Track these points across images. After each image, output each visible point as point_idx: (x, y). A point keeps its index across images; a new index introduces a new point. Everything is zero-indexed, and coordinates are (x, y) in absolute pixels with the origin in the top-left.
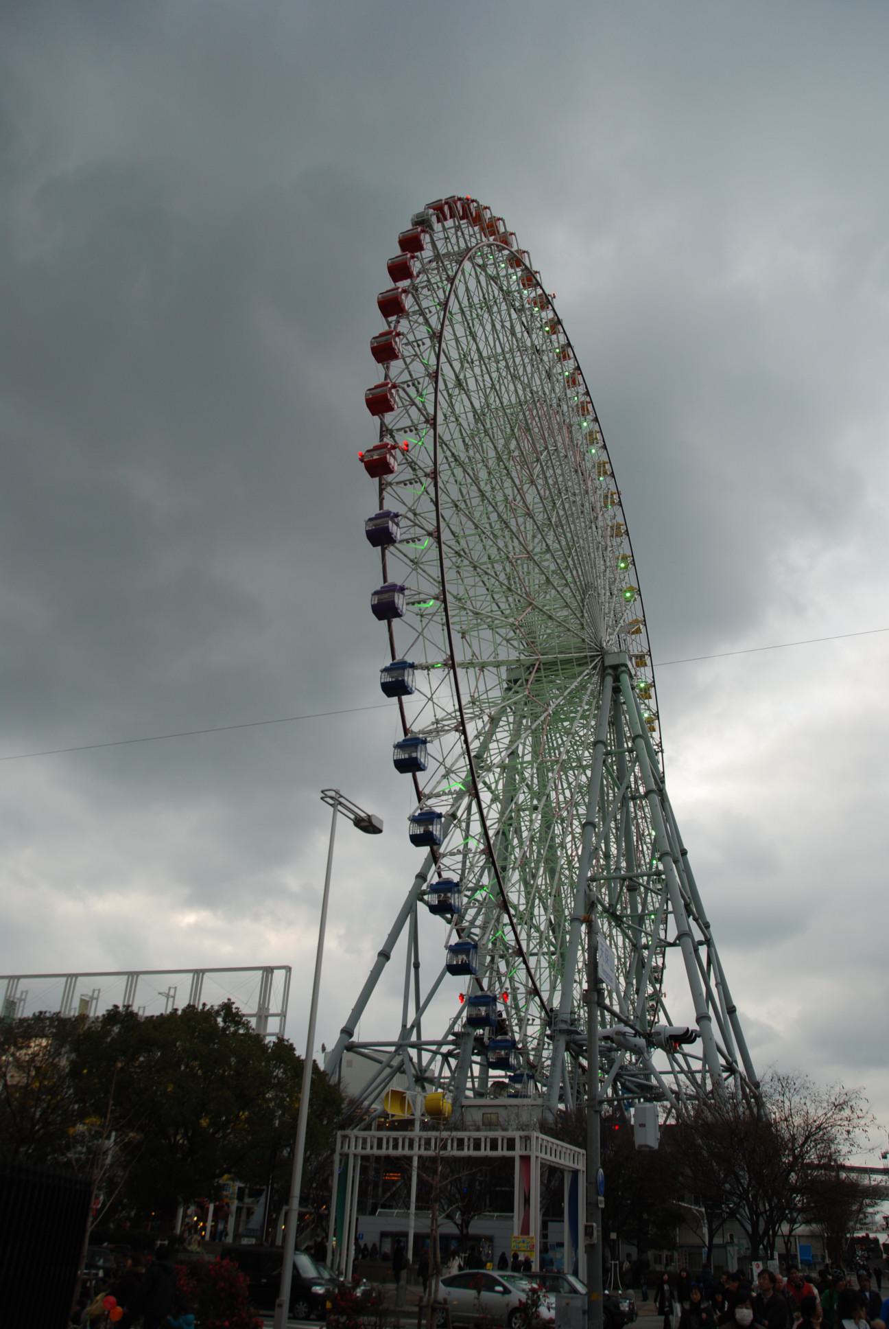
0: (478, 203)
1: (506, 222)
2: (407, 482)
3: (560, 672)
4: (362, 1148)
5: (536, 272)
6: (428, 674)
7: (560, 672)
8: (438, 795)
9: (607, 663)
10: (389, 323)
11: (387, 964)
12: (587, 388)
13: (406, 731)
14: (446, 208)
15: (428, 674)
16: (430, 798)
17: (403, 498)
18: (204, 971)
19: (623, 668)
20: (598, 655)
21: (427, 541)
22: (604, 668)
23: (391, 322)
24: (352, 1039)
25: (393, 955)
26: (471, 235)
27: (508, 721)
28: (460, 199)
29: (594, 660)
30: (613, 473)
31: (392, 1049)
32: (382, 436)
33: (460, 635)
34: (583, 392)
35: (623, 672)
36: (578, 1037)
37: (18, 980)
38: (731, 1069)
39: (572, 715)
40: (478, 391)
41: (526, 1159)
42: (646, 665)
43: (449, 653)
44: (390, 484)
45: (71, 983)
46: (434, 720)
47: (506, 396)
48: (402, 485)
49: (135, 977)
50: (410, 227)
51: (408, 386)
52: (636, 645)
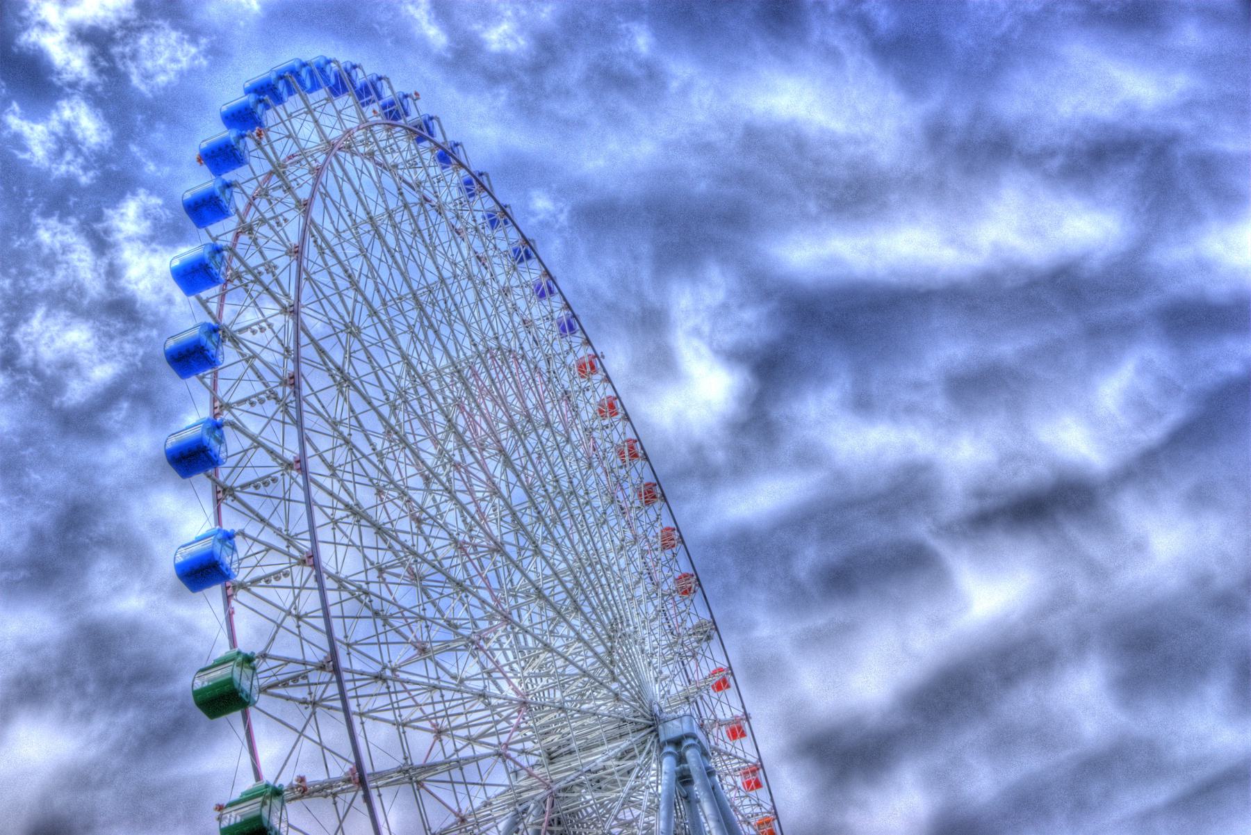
10: (204, 303)
12: (565, 299)
19: (690, 741)
23: (207, 300)
27: (443, 717)
28: (304, 65)
30: (645, 454)
34: (560, 306)
42: (728, 687)
43: (353, 759)
47: (428, 446)
48: (251, 489)
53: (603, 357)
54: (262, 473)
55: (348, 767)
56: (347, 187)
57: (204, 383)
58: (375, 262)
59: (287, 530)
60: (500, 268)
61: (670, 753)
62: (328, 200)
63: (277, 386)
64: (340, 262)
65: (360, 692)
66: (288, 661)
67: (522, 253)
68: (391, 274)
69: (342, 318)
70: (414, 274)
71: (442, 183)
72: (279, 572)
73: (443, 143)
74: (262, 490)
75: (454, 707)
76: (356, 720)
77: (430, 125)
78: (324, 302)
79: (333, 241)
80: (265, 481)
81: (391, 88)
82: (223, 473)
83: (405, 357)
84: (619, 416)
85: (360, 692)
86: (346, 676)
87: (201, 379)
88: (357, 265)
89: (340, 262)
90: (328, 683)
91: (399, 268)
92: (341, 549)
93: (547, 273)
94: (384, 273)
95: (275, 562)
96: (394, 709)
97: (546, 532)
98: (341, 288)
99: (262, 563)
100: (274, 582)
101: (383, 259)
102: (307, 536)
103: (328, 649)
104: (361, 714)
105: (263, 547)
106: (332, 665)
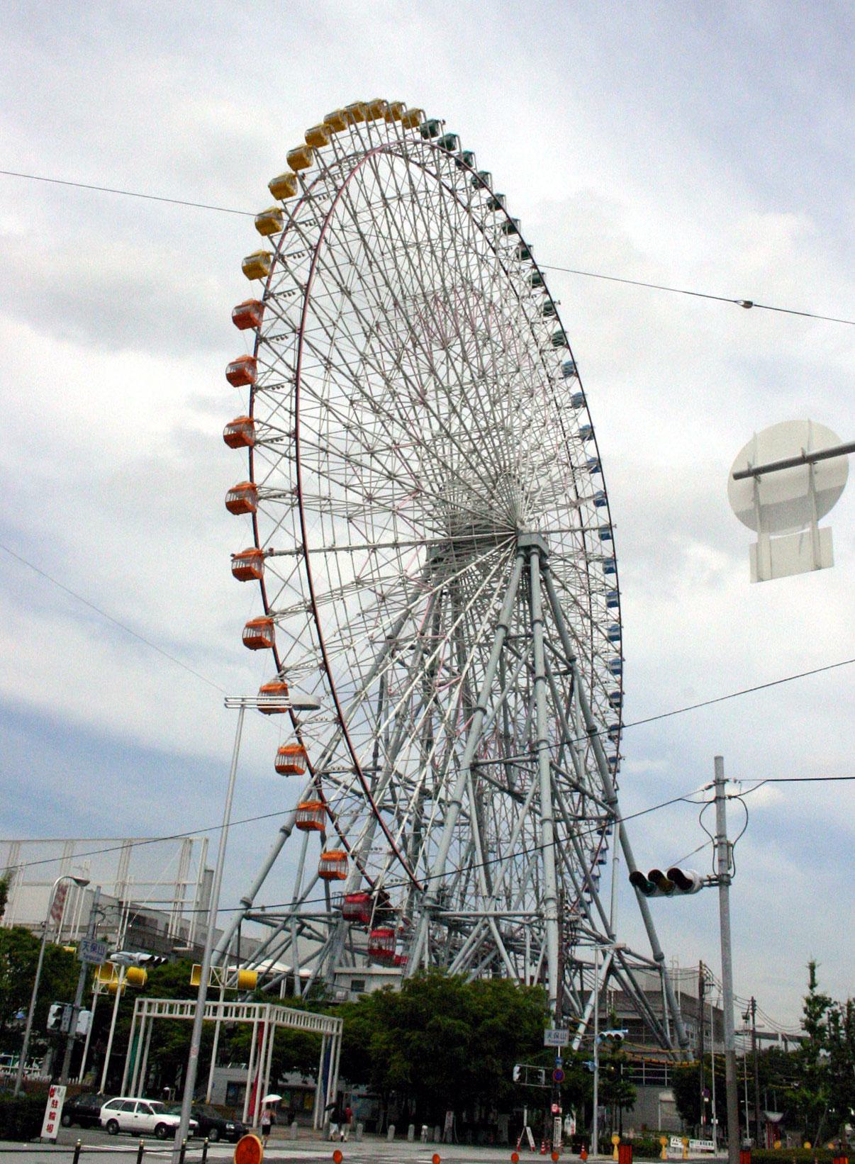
0: (387, 103)
3: (476, 550)
7: (476, 550)
17: (313, 389)
20: (512, 535)
21: (287, 440)
22: (518, 549)
26: (385, 133)
33: (346, 520)
39: (490, 592)
40: (364, 290)
41: (261, 1025)
58: (403, 274)
61: (522, 556)
64: (381, 271)
68: (362, 175)
70: (427, 282)
73: (465, 406)
74: (276, 390)
78: (368, 292)
79: (379, 258)
81: (425, 116)
82: (568, 396)
89: (381, 271)
97: (512, 953)
98: (379, 284)
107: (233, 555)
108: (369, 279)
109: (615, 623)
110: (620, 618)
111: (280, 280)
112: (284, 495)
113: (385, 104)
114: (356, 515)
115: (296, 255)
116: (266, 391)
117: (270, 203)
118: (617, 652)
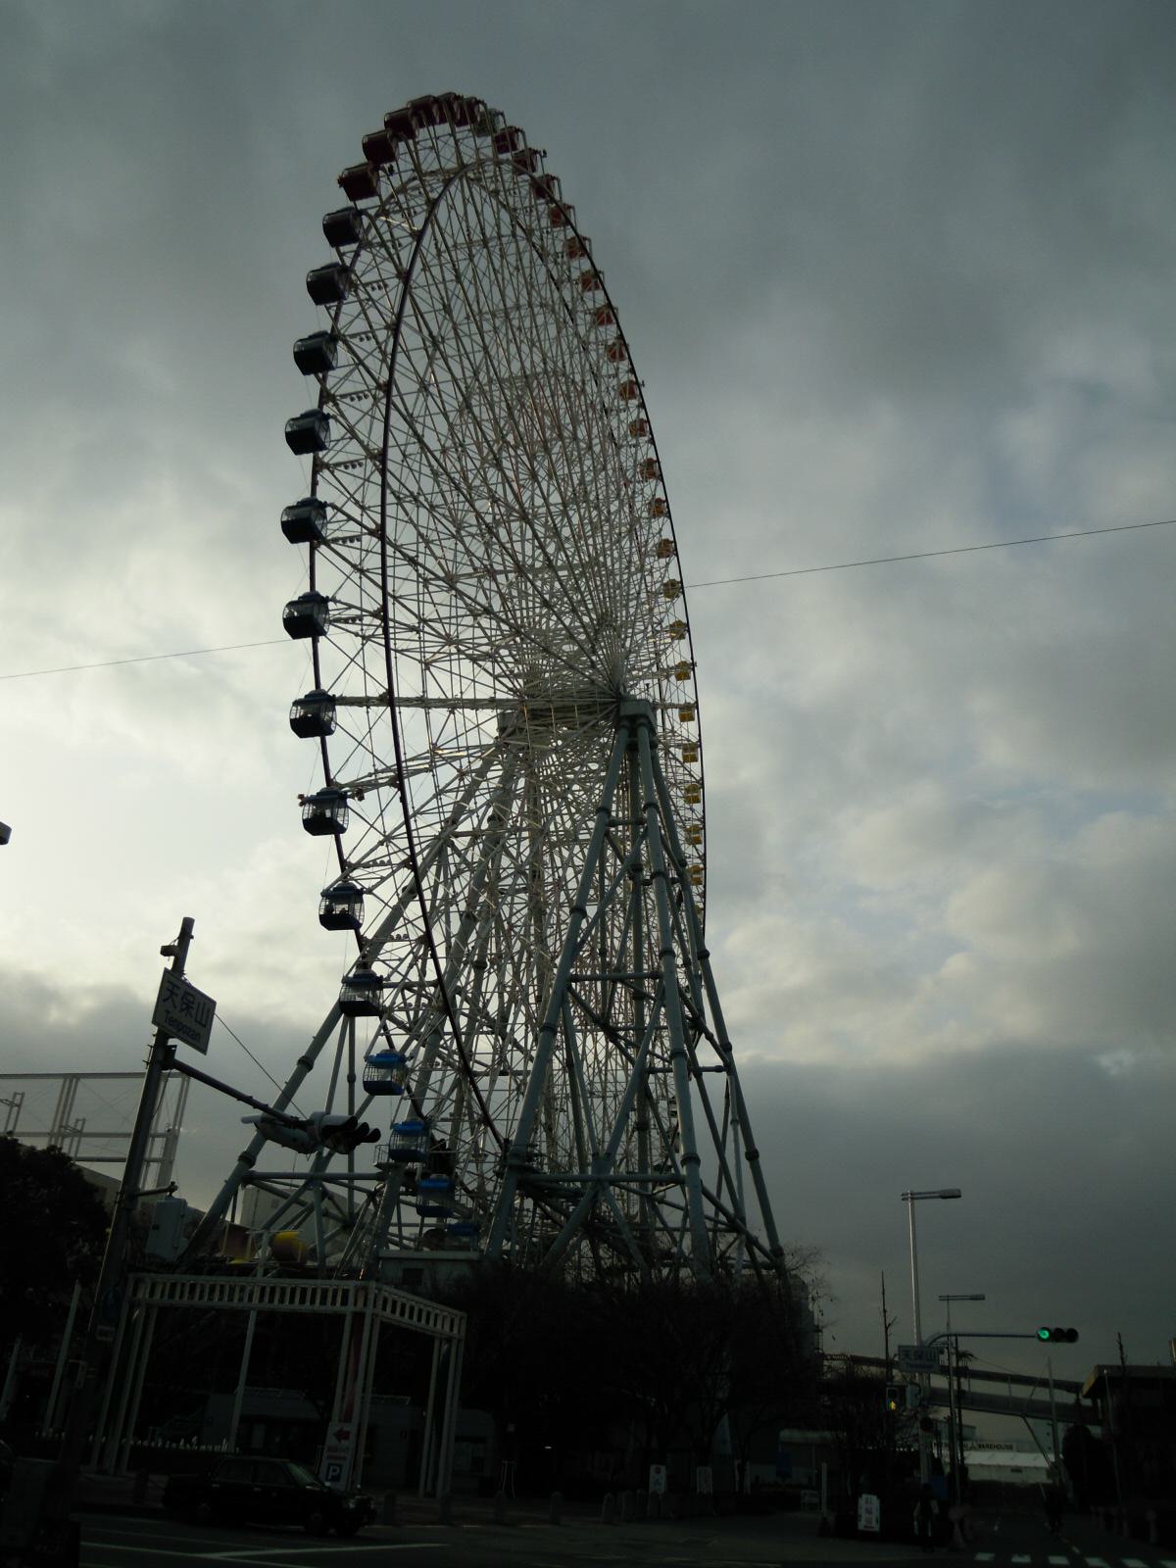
0: (485, 105)
1: (526, 134)
2: (356, 463)
4: (321, 1304)
5: (569, 207)
6: (368, 712)
8: (367, 866)
9: (622, 713)
10: (341, 255)
11: (308, 1074)
13: (329, 780)
14: (435, 110)
15: (368, 712)
16: (355, 869)
18: (77, 1077)
19: (643, 720)
23: (344, 254)
24: (253, 1169)
25: (317, 1062)
26: (475, 146)
28: (458, 98)
29: (607, 708)
31: (301, 1182)
32: (321, 404)
35: (642, 724)
36: (533, 1176)
37: (78, 1079)
38: (736, 1224)
41: (359, 1317)
44: (327, 466)
45: (70, 1087)
46: (373, 771)
49: (74, 1080)
50: (382, 127)
51: (361, 340)
52: (680, 692)
53: (643, 385)
54: (352, 458)
55: (382, 691)
56: (470, 208)
57: (329, 313)
59: (363, 502)
60: (583, 321)
62: (453, 212)
63: (380, 329)
65: (397, 636)
66: (350, 607)
67: (605, 315)
69: (442, 298)
71: (550, 236)
72: (354, 537)
74: (350, 470)
75: (465, 349)
76: (393, 653)
77: (551, 184)
80: (353, 464)
83: (485, 348)
84: (646, 438)
85: (397, 636)
86: (391, 624)
87: (328, 309)
88: (462, 266)
90: (378, 627)
91: (499, 286)
92: (401, 525)
93: (621, 337)
94: (486, 283)
95: (352, 528)
96: (421, 652)
99: (342, 528)
100: (348, 543)
101: (487, 274)
102: (379, 509)
103: (381, 603)
104: (396, 651)
105: (345, 518)
106: (382, 614)
107: (301, 797)
108: (436, 271)
109: (698, 823)
110: (704, 817)
111: (343, 377)
112: (361, 618)
113: (482, 108)
114: (435, 661)
115: (363, 336)
116: (333, 545)
117: (340, 200)
118: (700, 857)
